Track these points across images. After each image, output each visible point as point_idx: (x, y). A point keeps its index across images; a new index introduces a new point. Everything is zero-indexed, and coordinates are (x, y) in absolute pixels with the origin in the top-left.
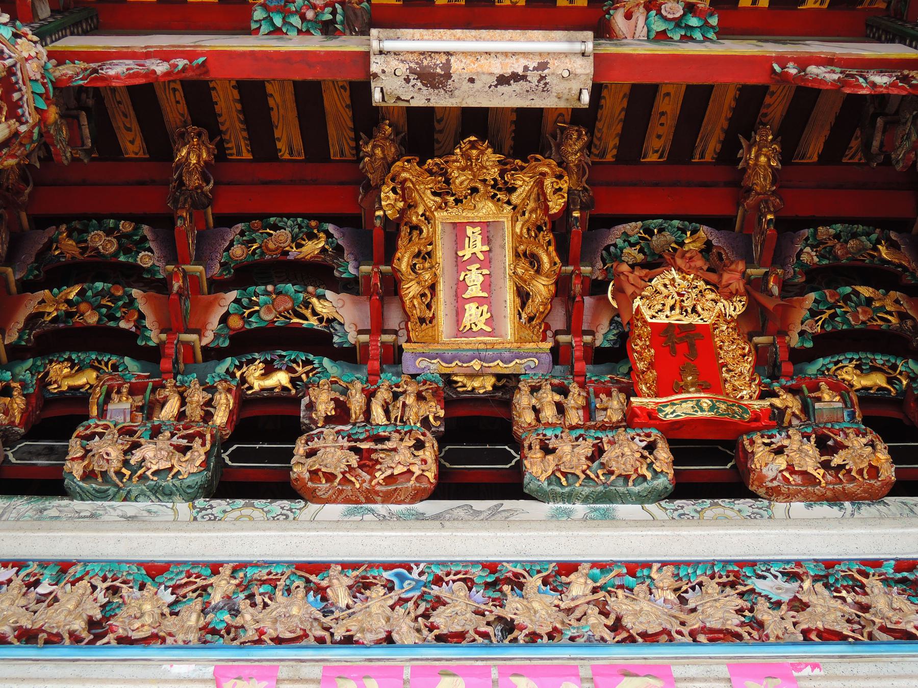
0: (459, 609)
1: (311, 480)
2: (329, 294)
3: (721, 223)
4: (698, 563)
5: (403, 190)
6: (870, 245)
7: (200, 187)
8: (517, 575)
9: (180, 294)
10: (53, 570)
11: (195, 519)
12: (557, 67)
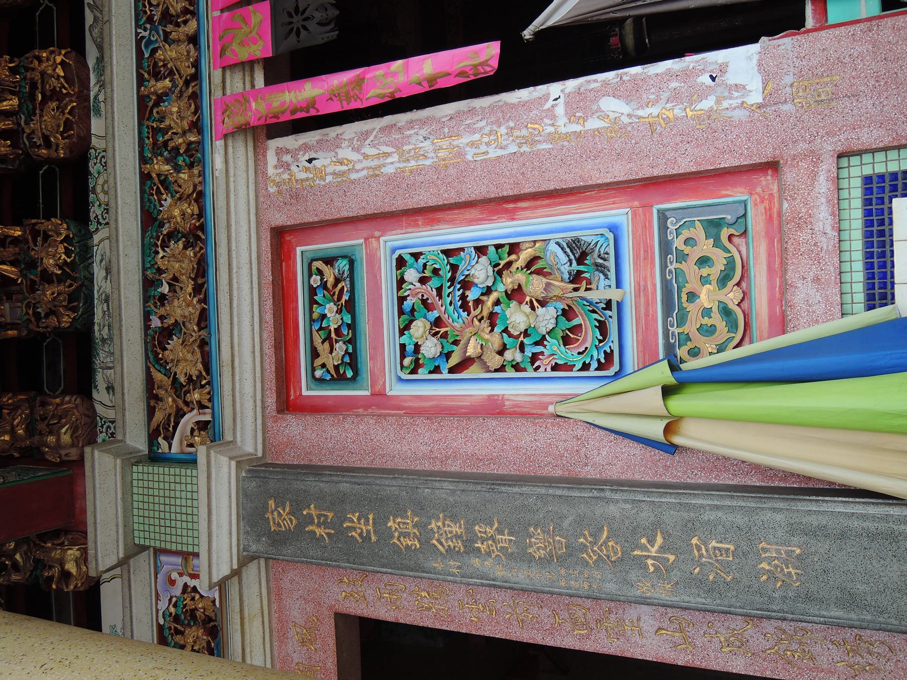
11: (107, 224)
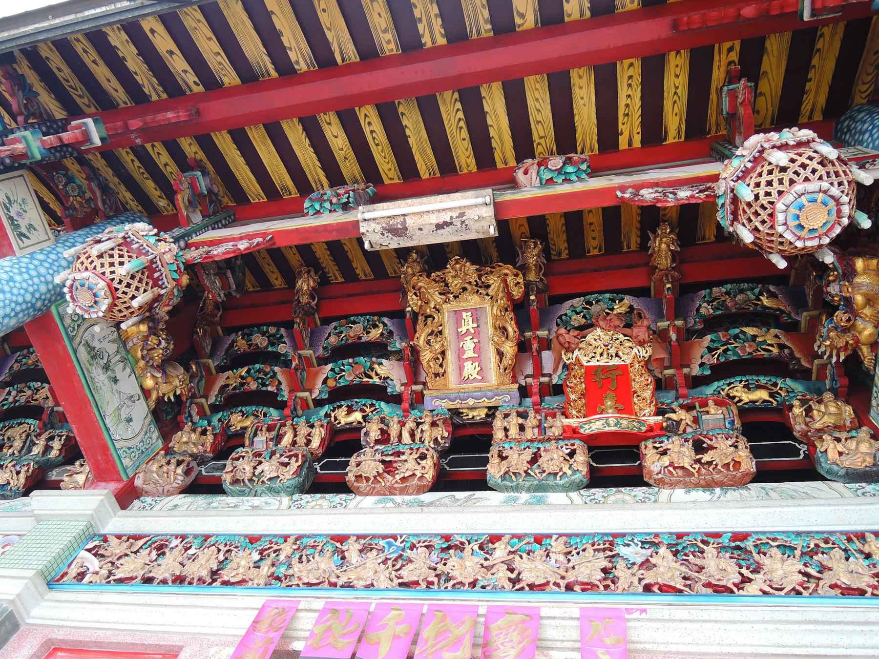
0: (419, 566)
1: (357, 481)
2: (384, 361)
3: (640, 292)
4: (585, 535)
5: (418, 292)
6: (753, 297)
7: (309, 303)
8: (462, 543)
9: (296, 369)
10: (198, 541)
12: (471, 214)
